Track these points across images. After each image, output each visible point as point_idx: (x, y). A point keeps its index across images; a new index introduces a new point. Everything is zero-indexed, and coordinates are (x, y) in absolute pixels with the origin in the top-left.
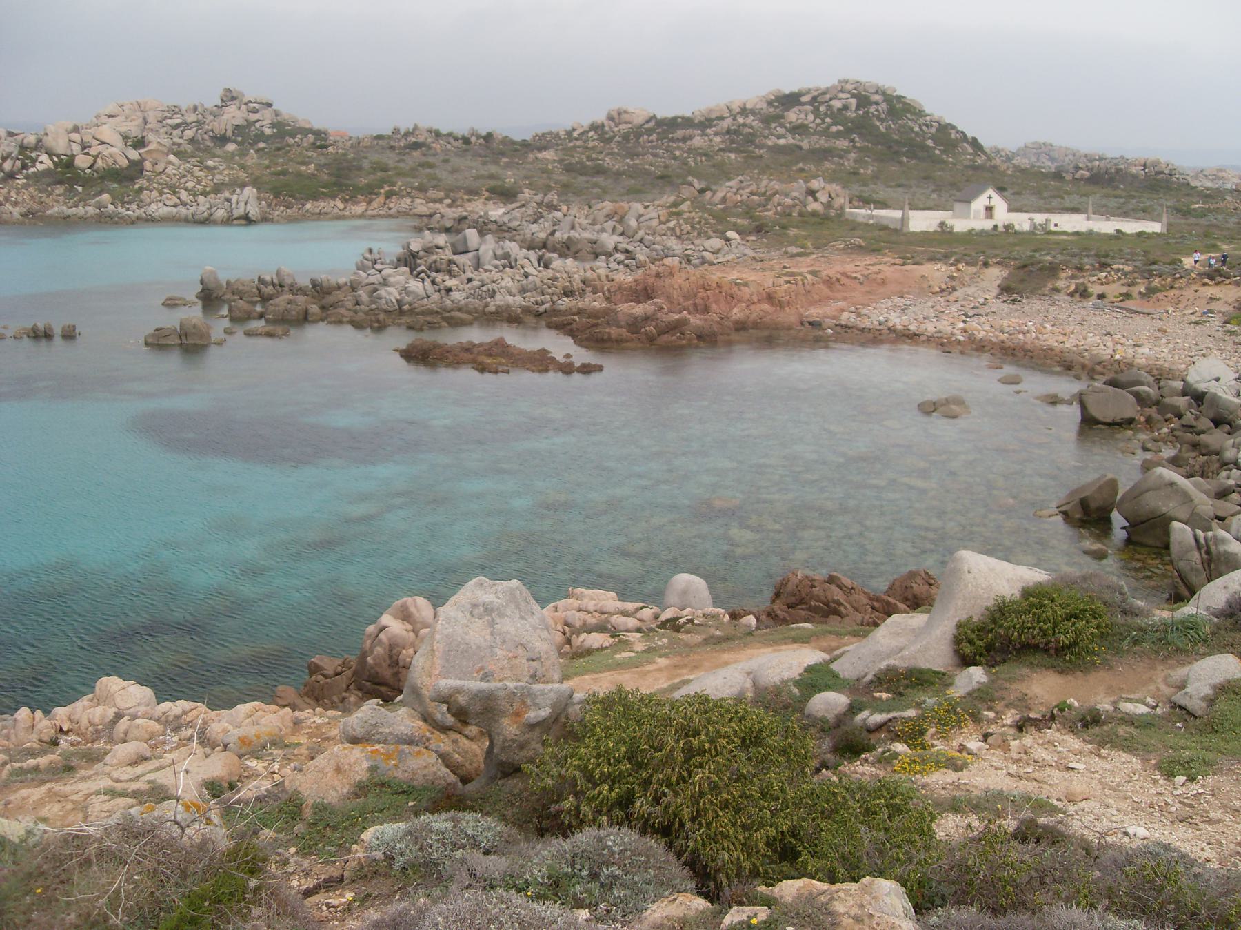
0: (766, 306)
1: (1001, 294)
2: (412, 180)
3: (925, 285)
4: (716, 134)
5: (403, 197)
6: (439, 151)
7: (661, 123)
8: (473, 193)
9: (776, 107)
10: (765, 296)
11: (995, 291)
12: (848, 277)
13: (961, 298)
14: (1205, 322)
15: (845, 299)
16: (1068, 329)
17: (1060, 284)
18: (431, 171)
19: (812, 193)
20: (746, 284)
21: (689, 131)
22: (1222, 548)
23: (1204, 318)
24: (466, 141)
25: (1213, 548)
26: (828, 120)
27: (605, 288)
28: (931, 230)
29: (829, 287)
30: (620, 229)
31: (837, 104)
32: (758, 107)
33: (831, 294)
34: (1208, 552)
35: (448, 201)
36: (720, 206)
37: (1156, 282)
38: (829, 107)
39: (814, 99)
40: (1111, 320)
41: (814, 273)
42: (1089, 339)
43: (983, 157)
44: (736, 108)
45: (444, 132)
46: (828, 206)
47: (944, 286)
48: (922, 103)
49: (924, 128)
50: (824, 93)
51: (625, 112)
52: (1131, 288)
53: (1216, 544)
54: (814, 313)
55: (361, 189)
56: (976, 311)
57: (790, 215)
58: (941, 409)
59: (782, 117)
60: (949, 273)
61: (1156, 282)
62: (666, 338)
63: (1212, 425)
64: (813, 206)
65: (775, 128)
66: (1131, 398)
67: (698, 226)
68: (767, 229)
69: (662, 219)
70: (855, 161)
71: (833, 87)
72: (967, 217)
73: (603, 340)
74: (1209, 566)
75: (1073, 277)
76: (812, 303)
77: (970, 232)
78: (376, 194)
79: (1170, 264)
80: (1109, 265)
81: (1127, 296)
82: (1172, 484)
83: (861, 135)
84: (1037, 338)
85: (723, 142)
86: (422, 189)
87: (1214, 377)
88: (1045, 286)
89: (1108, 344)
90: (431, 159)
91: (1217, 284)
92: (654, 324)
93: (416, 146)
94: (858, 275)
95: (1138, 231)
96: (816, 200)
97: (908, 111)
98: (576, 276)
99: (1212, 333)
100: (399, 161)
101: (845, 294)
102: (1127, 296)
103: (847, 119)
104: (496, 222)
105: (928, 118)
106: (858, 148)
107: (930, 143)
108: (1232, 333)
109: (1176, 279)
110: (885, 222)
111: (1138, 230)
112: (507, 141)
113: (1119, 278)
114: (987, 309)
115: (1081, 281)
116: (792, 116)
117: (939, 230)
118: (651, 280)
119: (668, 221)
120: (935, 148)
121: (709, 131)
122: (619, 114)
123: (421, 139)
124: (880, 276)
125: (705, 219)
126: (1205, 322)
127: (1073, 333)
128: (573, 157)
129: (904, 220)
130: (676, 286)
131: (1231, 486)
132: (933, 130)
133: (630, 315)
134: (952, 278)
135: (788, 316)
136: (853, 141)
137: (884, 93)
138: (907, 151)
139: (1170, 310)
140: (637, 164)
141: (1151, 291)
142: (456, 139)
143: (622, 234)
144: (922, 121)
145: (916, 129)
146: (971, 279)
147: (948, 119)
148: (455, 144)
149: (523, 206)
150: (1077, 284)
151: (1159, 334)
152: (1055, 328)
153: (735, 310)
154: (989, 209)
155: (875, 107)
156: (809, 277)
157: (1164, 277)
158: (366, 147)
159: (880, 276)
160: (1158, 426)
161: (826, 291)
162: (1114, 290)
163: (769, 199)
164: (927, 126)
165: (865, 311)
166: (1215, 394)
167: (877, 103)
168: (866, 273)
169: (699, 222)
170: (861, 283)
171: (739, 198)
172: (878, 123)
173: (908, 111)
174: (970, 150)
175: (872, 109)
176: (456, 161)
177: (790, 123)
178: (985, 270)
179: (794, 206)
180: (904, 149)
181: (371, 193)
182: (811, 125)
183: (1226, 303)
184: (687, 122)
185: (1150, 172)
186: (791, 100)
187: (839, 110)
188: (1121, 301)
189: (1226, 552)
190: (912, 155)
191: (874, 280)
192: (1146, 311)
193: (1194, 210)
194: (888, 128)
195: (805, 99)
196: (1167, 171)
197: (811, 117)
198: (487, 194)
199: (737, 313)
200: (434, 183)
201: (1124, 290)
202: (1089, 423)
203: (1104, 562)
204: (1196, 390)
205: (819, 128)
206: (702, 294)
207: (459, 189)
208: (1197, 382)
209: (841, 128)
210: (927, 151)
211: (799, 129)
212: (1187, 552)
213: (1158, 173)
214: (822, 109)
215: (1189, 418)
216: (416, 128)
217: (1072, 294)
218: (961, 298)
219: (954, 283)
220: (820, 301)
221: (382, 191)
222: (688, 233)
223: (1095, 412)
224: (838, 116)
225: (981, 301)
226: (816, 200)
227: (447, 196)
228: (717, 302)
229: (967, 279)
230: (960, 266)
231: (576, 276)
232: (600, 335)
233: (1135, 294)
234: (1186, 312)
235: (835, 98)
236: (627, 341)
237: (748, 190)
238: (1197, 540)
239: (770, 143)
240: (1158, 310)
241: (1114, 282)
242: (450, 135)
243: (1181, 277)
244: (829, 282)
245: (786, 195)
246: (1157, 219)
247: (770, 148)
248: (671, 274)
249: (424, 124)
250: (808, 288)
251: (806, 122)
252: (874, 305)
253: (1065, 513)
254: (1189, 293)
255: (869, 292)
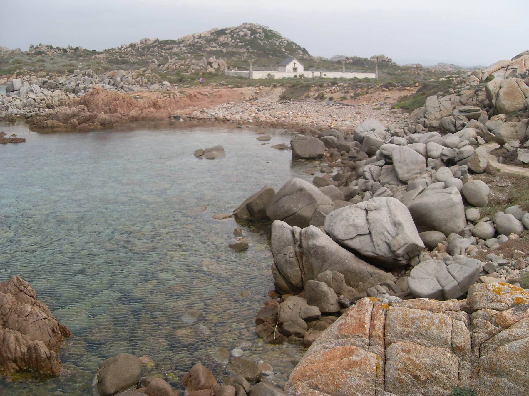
0: (152, 109)
1: (281, 100)
2: (31, 67)
3: (242, 98)
4: (184, 46)
5: (26, 75)
6: (50, 55)
7: (160, 43)
8: (61, 72)
9: (215, 36)
10: (152, 104)
11: (278, 99)
12: (201, 94)
13: (259, 103)
14: (382, 108)
15: (198, 105)
16: (310, 114)
17: (311, 94)
18: (43, 64)
19: (210, 64)
20: (142, 98)
21: (172, 45)
22: (311, 242)
23: (382, 107)
24: (65, 51)
25: (304, 242)
26: (237, 40)
27: (67, 103)
28: (264, 78)
29: (190, 99)
30: (112, 82)
31: (242, 34)
32: (206, 35)
33: (191, 103)
34: (300, 246)
35: (48, 77)
36: (165, 71)
37: (359, 91)
38: (238, 35)
39: (232, 31)
40: (334, 110)
41: (181, 92)
42: (319, 119)
43: (307, 56)
44: (197, 36)
45: (54, 47)
46: (218, 70)
47: (251, 97)
48: (280, 32)
49: (281, 44)
50: (236, 29)
51: (148, 40)
52: (346, 94)
53: (307, 238)
54: (178, 112)
55: (5, 71)
56: (265, 108)
57: (198, 74)
58: (207, 154)
59: (217, 40)
60: (255, 91)
61: (359, 91)
62: (82, 125)
63: (367, 156)
64: (210, 70)
65: (212, 44)
66: (321, 143)
67: (151, 80)
68: (184, 80)
69: (134, 77)
70: (247, 57)
71: (241, 26)
72: (285, 71)
73: (44, 127)
74: (302, 258)
75: (317, 90)
76: (179, 108)
77: (283, 79)
78: (12, 74)
79: (367, 82)
80: (336, 84)
81: (344, 98)
82: (302, 190)
83: (252, 47)
84: (292, 119)
85: (186, 49)
86: (35, 71)
87: (372, 128)
88: (303, 95)
89: (328, 121)
90: (45, 59)
91: (390, 90)
92: (77, 118)
93: (40, 53)
94: (207, 93)
95: (364, 77)
96: (212, 67)
97: (274, 36)
98: (56, 98)
99: (385, 113)
100: (28, 59)
101: (198, 103)
102: (344, 98)
103: (246, 40)
104: (62, 83)
105: (283, 39)
106: (250, 52)
107: (283, 50)
108: (394, 113)
109: (369, 89)
110: (242, 75)
111: (364, 77)
112: (86, 51)
113: (341, 90)
114: (271, 107)
115: (322, 92)
116: (222, 39)
117: (268, 78)
118: (87, 97)
119: (137, 78)
120: (285, 52)
121: (181, 45)
122: (146, 41)
123: (42, 50)
124: (219, 93)
125: (156, 77)
126: (382, 108)
127: (312, 116)
128: (113, 56)
129: (250, 74)
130: (100, 100)
131: (355, 190)
132: (285, 45)
133: (65, 114)
134: (256, 93)
135: (163, 113)
136: (248, 49)
137: (263, 29)
138: (272, 53)
139: (365, 103)
140: (143, 59)
141: (356, 95)
142: (60, 50)
143: (113, 85)
144: (280, 40)
145: (277, 44)
146: (266, 94)
147: (292, 40)
148: (59, 52)
149: (76, 75)
150: (319, 93)
151: (357, 115)
152: (303, 114)
153: (133, 111)
154: (295, 69)
155: (259, 34)
156: (178, 94)
157: (363, 88)
158: (15, 54)
159: (219, 93)
160: (336, 158)
161: (188, 101)
162: (337, 96)
163: (189, 67)
164: (282, 43)
165: (206, 110)
166: (368, 137)
167: (260, 33)
168: (211, 92)
169: (152, 78)
170: (208, 97)
171: (174, 67)
172: (260, 42)
173: (274, 36)
174: (302, 53)
175: (258, 35)
176: (57, 59)
177: (220, 42)
178: (275, 89)
179: (201, 70)
180: (271, 53)
181: (9, 74)
182: (230, 43)
183: (394, 99)
184: (173, 42)
185: (380, 60)
186: (222, 32)
187: (243, 36)
188: (341, 101)
189: (315, 246)
190: (274, 55)
191: (215, 95)
192: (352, 104)
193: (396, 74)
194: (265, 43)
195: (227, 32)
196: (387, 60)
197: (230, 39)
198: (68, 73)
199: (133, 113)
200: (41, 68)
201: (343, 95)
202: (296, 158)
203: (244, 254)
204: (360, 136)
205: (233, 44)
206: (114, 102)
207: (54, 71)
208: (361, 132)
209: (243, 44)
210: (282, 53)
211: (225, 45)
212: (285, 246)
213: (383, 61)
214: (235, 36)
215: (353, 152)
216: (40, 45)
217: (316, 98)
218: (259, 103)
219: (257, 96)
220: (185, 106)
221: (15, 72)
222: (146, 83)
223: (301, 152)
224: (242, 39)
225: (269, 103)
226: (212, 67)
227: (48, 74)
228: (122, 107)
229: (264, 93)
230: (261, 87)
231: (56, 98)
232: (41, 125)
233: (348, 97)
234: (373, 104)
235: (241, 31)
236: (58, 127)
237: (179, 63)
238: (293, 235)
239: (208, 50)
240: (359, 104)
241: (338, 91)
242: (57, 48)
243: (372, 88)
244: (190, 97)
245: (197, 65)
246: (373, 72)
247: (208, 52)
248: (98, 93)
249: (45, 43)
250: (177, 99)
251: (227, 42)
252: (212, 107)
253: (236, 215)
254: (375, 95)
255: (212, 102)
